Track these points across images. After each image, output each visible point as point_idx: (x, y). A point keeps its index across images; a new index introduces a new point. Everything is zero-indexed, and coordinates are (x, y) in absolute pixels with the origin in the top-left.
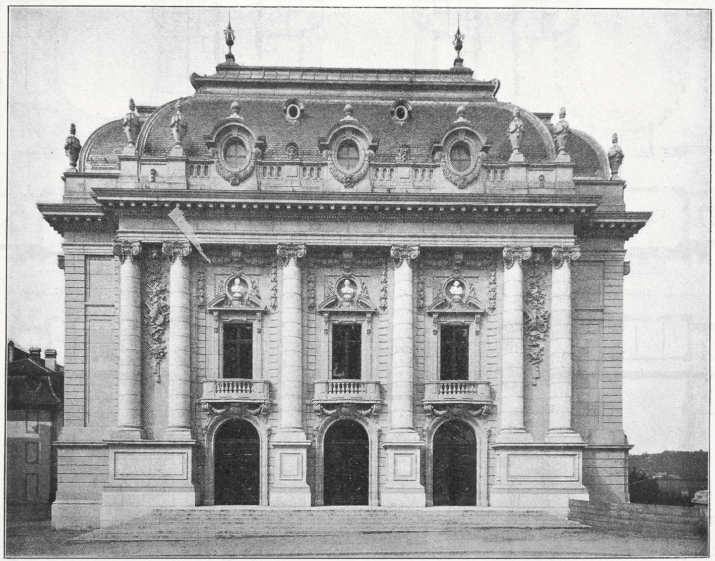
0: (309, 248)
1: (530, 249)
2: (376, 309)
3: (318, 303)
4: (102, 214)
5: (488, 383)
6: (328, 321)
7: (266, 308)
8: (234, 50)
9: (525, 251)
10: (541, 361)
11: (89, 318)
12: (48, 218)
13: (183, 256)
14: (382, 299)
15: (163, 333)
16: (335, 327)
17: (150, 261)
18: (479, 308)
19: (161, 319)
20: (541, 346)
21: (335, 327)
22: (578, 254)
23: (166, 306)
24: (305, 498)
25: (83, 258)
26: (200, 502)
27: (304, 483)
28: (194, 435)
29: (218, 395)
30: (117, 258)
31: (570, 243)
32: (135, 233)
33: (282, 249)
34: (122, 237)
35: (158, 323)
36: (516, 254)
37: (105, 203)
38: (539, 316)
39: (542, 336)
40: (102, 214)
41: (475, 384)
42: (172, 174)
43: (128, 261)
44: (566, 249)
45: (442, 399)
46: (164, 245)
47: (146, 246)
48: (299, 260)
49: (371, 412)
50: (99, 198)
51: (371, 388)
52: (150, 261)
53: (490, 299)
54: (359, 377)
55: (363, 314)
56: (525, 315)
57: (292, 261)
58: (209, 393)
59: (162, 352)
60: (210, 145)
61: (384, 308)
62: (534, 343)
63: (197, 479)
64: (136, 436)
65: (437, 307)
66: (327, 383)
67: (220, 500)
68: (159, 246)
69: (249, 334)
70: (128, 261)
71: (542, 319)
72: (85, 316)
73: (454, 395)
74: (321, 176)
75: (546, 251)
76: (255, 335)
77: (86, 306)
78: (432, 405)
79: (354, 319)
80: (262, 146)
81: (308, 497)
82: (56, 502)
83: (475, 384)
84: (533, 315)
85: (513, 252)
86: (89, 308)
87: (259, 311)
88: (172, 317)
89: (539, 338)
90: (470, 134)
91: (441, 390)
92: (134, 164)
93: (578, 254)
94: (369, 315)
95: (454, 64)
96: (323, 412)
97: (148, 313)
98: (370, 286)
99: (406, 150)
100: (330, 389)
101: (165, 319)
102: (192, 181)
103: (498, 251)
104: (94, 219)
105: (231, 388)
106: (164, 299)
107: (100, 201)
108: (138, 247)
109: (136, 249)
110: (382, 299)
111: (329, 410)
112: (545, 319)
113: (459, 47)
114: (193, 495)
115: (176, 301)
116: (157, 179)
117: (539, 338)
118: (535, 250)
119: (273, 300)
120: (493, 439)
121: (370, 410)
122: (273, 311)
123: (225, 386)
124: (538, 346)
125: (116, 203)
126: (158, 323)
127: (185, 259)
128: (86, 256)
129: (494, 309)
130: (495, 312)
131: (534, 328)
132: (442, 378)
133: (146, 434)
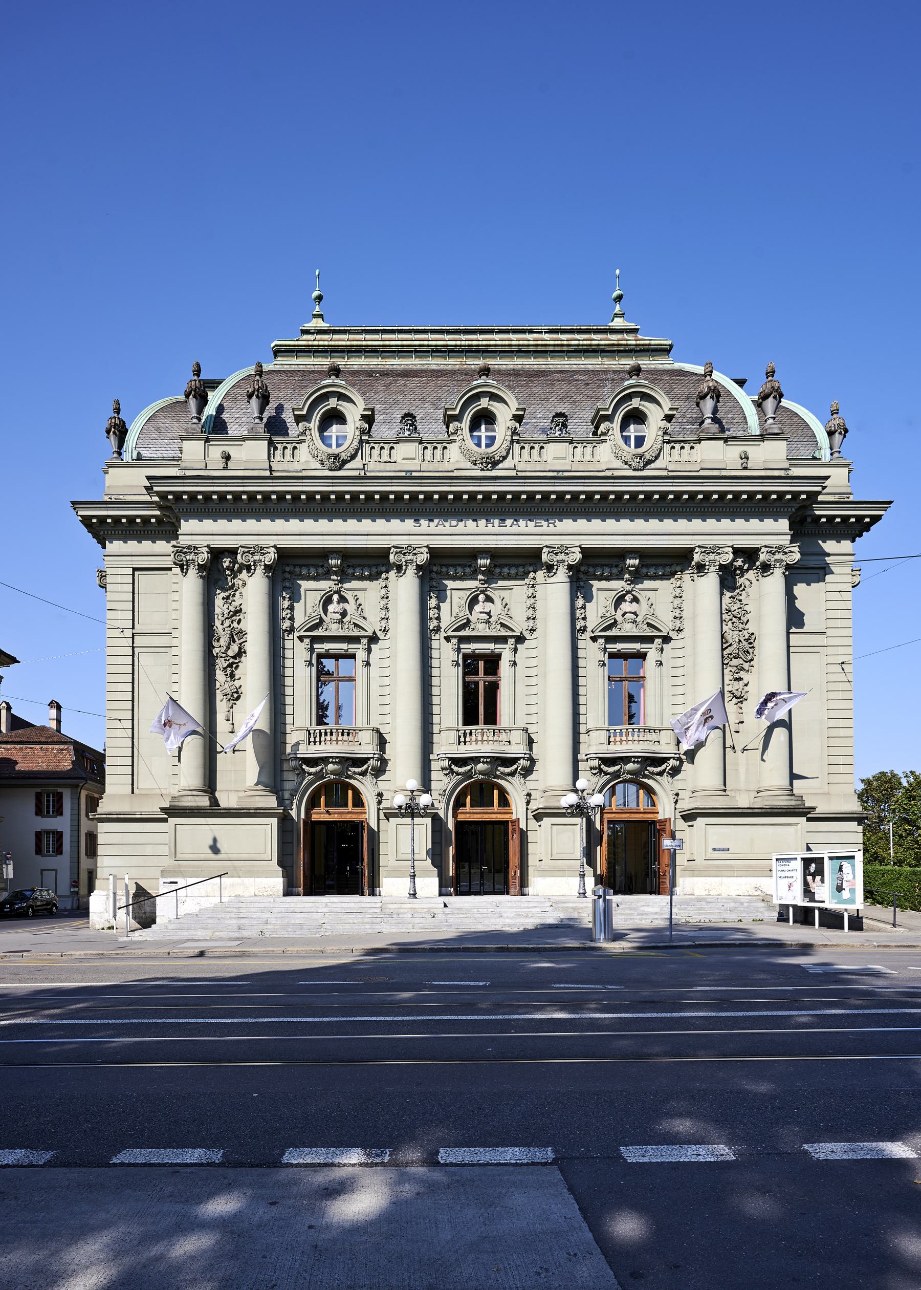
0: (433, 551)
1: (730, 549)
2: (374, 633)
3: (443, 625)
4: (158, 513)
5: (526, 730)
7: (374, 633)
9: (791, 552)
12: (86, 521)
13: (265, 565)
15: (237, 667)
16: (466, 657)
17: (217, 571)
18: (661, 631)
19: (235, 648)
21: (466, 657)
22: (797, 556)
23: (241, 631)
24: (429, 884)
25: (130, 571)
26: (288, 893)
28: (281, 801)
29: (462, 748)
30: (177, 570)
31: (785, 540)
32: (200, 533)
34: (184, 541)
35: (230, 653)
36: (257, 557)
37: (163, 496)
39: (746, 666)
40: (158, 513)
42: (251, 455)
43: (193, 572)
44: (780, 549)
46: (240, 550)
47: (217, 554)
48: (419, 568)
49: (517, 769)
50: (155, 489)
52: (217, 571)
53: (675, 618)
55: (503, 640)
58: (446, 745)
59: (237, 692)
60: (298, 419)
61: (385, 631)
62: (737, 676)
63: (285, 861)
64: (204, 802)
65: (311, 629)
67: (310, 891)
68: (232, 552)
71: (745, 643)
72: (133, 647)
73: (322, 747)
79: (491, 646)
80: (369, 419)
81: (278, 883)
82: (95, 892)
85: (556, 554)
87: (364, 637)
88: (248, 647)
89: (742, 669)
90: (646, 397)
93: (797, 556)
94: (658, 641)
96: (452, 770)
97: (218, 641)
98: (512, 599)
99: (561, 420)
101: (240, 648)
103: (384, 554)
104: (146, 519)
105: (317, 739)
106: (239, 622)
107: (158, 494)
108: (272, 555)
109: (203, 557)
111: (609, 767)
112: (751, 643)
114: (436, 880)
115: (255, 624)
116: (230, 465)
117: (742, 669)
118: (737, 552)
119: (384, 621)
122: (381, 637)
124: (741, 679)
125: (178, 496)
126: (230, 653)
127: (201, 568)
128: (134, 570)
129: (532, 630)
130: (681, 635)
133: (214, 802)
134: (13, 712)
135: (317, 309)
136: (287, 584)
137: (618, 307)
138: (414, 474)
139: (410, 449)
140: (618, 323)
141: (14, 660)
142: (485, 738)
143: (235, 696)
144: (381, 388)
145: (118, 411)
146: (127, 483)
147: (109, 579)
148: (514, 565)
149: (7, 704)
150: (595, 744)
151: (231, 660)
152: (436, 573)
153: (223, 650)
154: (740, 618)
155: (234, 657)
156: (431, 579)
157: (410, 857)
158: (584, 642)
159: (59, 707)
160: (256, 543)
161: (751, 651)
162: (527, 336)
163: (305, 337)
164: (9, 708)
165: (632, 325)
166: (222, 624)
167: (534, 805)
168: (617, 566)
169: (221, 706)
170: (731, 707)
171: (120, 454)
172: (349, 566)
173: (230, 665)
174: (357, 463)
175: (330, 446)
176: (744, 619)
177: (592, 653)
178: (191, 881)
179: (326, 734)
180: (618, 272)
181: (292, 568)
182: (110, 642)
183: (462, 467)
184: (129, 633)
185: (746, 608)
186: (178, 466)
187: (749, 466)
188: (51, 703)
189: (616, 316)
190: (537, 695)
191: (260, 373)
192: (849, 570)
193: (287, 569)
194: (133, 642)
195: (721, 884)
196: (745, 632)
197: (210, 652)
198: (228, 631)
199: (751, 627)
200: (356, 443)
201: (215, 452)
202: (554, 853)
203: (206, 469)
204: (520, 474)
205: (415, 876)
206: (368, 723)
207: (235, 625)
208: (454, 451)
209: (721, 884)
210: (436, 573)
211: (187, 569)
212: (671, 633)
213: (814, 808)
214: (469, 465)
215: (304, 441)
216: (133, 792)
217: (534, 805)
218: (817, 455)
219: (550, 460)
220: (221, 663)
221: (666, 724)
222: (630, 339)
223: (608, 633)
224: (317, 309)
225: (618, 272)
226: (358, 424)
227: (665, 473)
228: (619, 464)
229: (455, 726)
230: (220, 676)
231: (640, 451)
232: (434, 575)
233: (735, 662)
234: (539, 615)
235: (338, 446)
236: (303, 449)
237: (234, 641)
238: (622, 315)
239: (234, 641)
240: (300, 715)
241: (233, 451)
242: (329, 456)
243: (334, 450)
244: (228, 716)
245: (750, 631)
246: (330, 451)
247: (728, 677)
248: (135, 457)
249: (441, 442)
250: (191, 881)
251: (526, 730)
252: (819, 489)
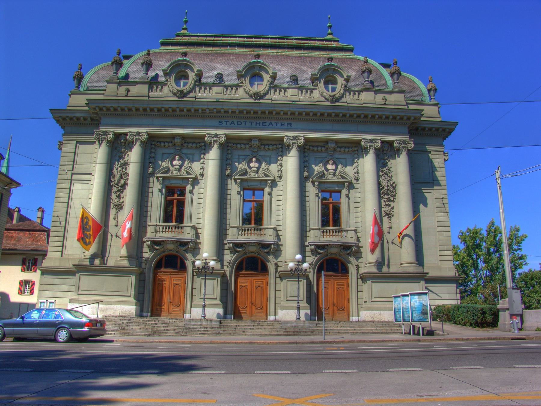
2: (274, 178)
5: (355, 231)
6: (162, 183)
10: (393, 216)
11: (73, 182)
14: (279, 171)
15: (122, 192)
19: (122, 182)
20: (392, 206)
22: (413, 146)
25: (75, 142)
27: (218, 302)
33: (131, 135)
35: (120, 185)
36: (293, 141)
38: (389, 185)
39: (392, 199)
41: (346, 231)
43: (104, 144)
44: (404, 142)
45: (162, 236)
48: (299, 147)
51: (350, 234)
54: (261, 225)
56: (379, 184)
57: (372, 151)
62: (387, 203)
66: (238, 228)
69: (183, 194)
70: (104, 144)
72: (71, 180)
74: (163, 91)
75: (391, 143)
76: (188, 195)
77: (73, 174)
78: (315, 245)
83: (346, 231)
84: (384, 183)
86: (74, 176)
91: (322, 234)
92: (115, 86)
100: (240, 233)
102: (151, 94)
109: (110, 137)
110: (355, 173)
115: (133, 170)
116: (129, 94)
118: (383, 142)
119: (280, 172)
120: (280, 269)
121: (187, 246)
123: (163, 229)
127: (109, 142)
128: (77, 142)
131: (385, 193)
132: (323, 225)
134: (21, 213)
135: (185, 26)
136: (153, 150)
137: (329, 31)
138: (220, 100)
139: (294, 91)
140: (329, 37)
141: (19, 184)
143: (120, 207)
144: (209, 61)
145: (80, 69)
146: (78, 102)
147: (63, 146)
149: (19, 208)
150: (313, 237)
152: (154, 145)
153: (116, 182)
154: (388, 175)
156: (228, 150)
157: (296, 298)
158: (309, 184)
159: (43, 212)
161: (394, 191)
162: (285, 41)
163: (177, 38)
164: (19, 211)
165: (336, 39)
166: (117, 169)
167: (362, 271)
168: (324, 147)
169: (113, 212)
170: (385, 219)
171: (79, 88)
172: (185, 142)
173: (119, 190)
174: (192, 95)
175: (329, 91)
176: (390, 175)
177: (234, 188)
178: (84, 305)
179: (327, 232)
180: (329, 16)
181: (156, 143)
182: (60, 177)
183: (245, 97)
184: (70, 173)
185: (391, 169)
186: (103, 94)
187: (387, 103)
188: (40, 208)
189: (329, 34)
190: (283, 209)
191: (149, 54)
192: (442, 153)
193: (153, 143)
194: (72, 177)
195: (380, 315)
196: (391, 182)
197: (109, 183)
198: (119, 173)
199: (394, 179)
200: (342, 91)
201: (123, 89)
202: (289, 295)
203: (117, 96)
204: (273, 102)
205: (299, 308)
206: (191, 222)
207: (124, 170)
208: (241, 91)
209: (380, 315)
210: (154, 145)
211: (102, 142)
212: (353, 180)
213: (428, 273)
214: (171, 95)
215: (241, 86)
216: (62, 256)
217: (362, 271)
218: (423, 99)
219: (214, 94)
220: (115, 189)
221: (352, 228)
222: (334, 44)
224: (185, 26)
225: (329, 16)
226: (269, 79)
228: (323, 99)
229: (237, 225)
230: (113, 196)
231: (333, 94)
232: (229, 148)
233: (386, 197)
234: (283, 169)
235: (184, 86)
236: (166, 88)
237: (122, 178)
238: (332, 34)
239: (122, 178)
240: (234, 218)
242: (178, 91)
243: (181, 88)
244: (115, 217)
245: (393, 181)
246: (179, 89)
247: (383, 204)
248: (85, 89)
249: (310, 89)
250: (84, 305)
251: (355, 231)
252: (420, 115)
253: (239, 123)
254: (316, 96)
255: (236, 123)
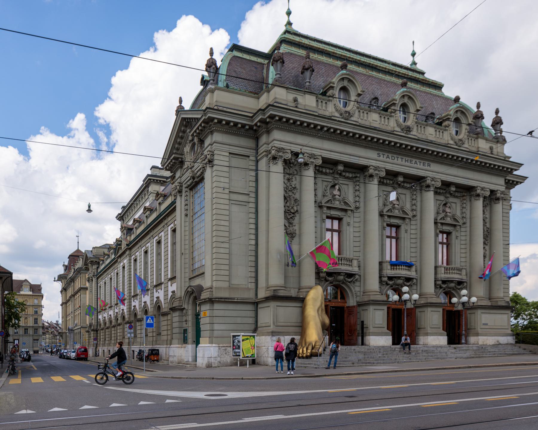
8: (292, 19)
32: (280, 139)
44: (502, 193)
95: (411, 65)
113: (289, 13)
142: (451, 272)
148: (351, 172)
151: (292, 215)
155: (293, 213)
160: (378, 165)
223: (327, 205)
227: (468, 150)
241: (300, 99)
253: (393, 158)
254: (391, 124)
255: (390, 157)
